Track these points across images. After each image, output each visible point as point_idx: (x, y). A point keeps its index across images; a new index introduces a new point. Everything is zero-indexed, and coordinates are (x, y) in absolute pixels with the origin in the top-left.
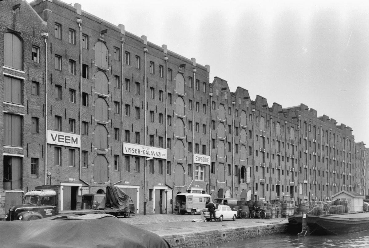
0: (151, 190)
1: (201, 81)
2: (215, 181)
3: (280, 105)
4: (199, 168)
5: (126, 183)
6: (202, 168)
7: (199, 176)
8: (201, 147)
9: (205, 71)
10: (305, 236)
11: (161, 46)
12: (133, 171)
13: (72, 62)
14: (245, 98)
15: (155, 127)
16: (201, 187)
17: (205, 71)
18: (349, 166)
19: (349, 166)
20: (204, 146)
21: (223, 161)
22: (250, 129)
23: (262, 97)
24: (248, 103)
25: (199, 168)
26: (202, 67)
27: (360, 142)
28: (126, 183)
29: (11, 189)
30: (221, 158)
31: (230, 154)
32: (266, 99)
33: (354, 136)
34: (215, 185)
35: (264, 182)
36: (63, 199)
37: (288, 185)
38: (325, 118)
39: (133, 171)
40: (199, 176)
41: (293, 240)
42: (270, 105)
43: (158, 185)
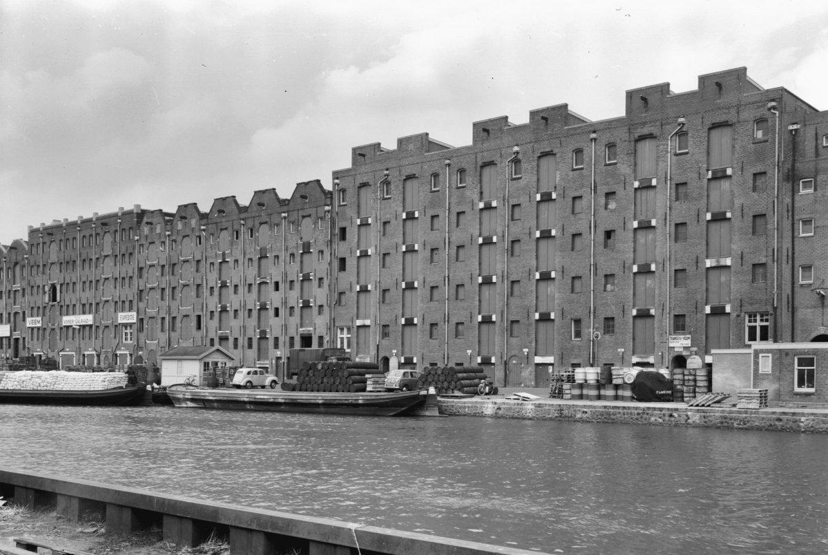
2: (143, 341)
3: (266, 190)
4: (129, 328)
5: (67, 350)
6: (131, 326)
7: (129, 336)
8: (127, 304)
12: (70, 339)
15: (88, 296)
16: (127, 349)
21: (154, 314)
23: (261, 191)
25: (129, 328)
28: (67, 350)
29: (793, 341)
30: (151, 312)
32: (740, 73)
33: (703, 80)
34: (144, 346)
35: (313, 332)
37: (294, 334)
39: (70, 339)
40: (129, 336)
41: (605, 532)
43: (88, 350)
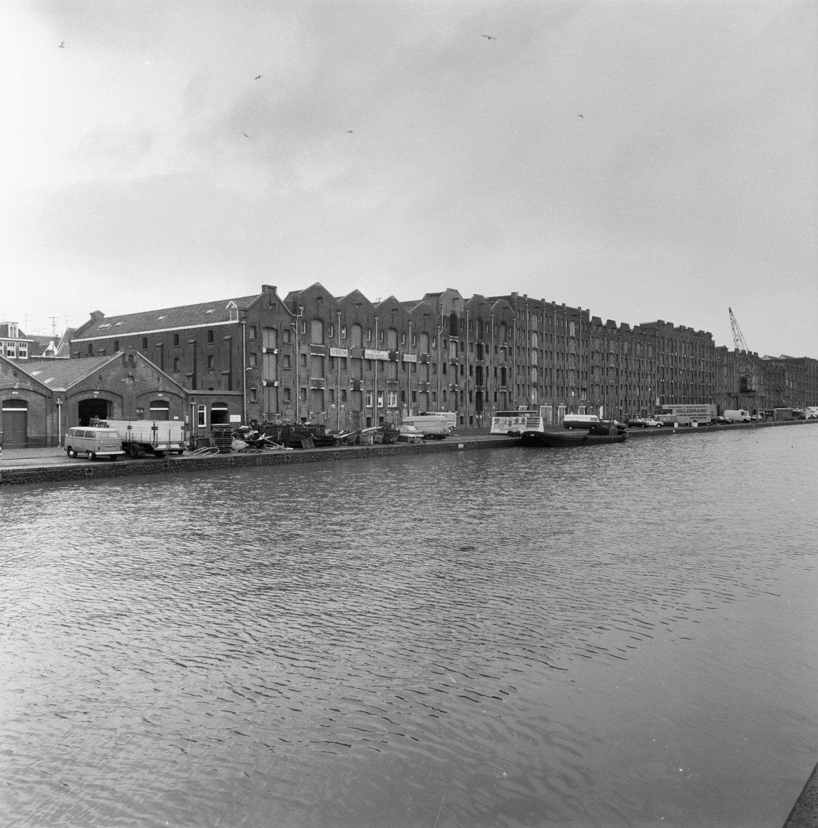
0: (557, 408)
1: (585, 323)
9: (587, 313)
10: (168, 407)
11: (561, 305)
13: (524, 330)
14: (598, 325)
17: (587, 313)
18: (669, 370)
19: (669, 370)
20: (586, 373)
22: (617, 353)
24: (615, 331)
26: (538, 301)
27: (722, 345)
31: (602, 377)
32: (709, 335)
36: (580, 420)
38: (682, 328)
42: (618, 326)
